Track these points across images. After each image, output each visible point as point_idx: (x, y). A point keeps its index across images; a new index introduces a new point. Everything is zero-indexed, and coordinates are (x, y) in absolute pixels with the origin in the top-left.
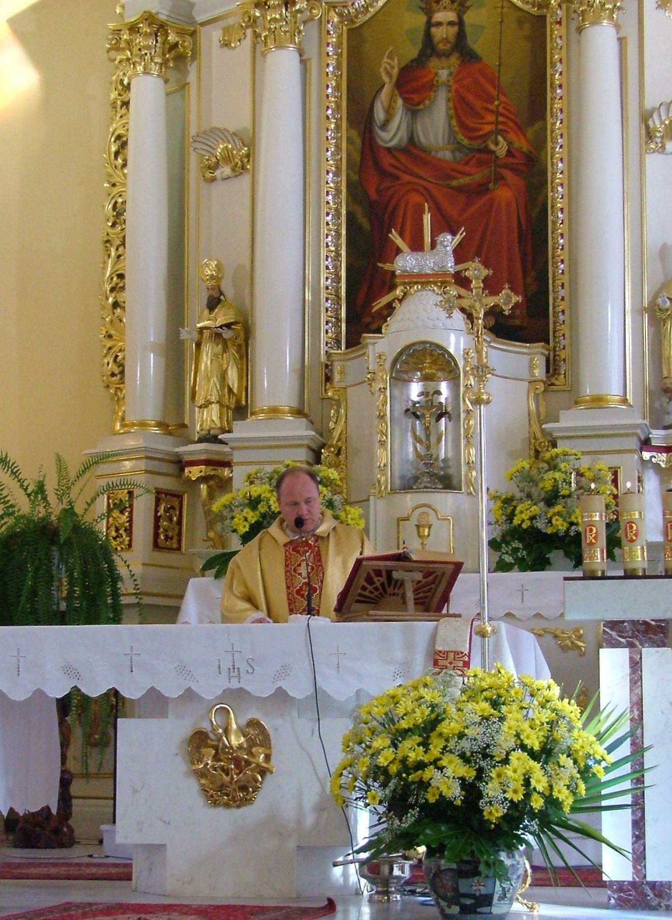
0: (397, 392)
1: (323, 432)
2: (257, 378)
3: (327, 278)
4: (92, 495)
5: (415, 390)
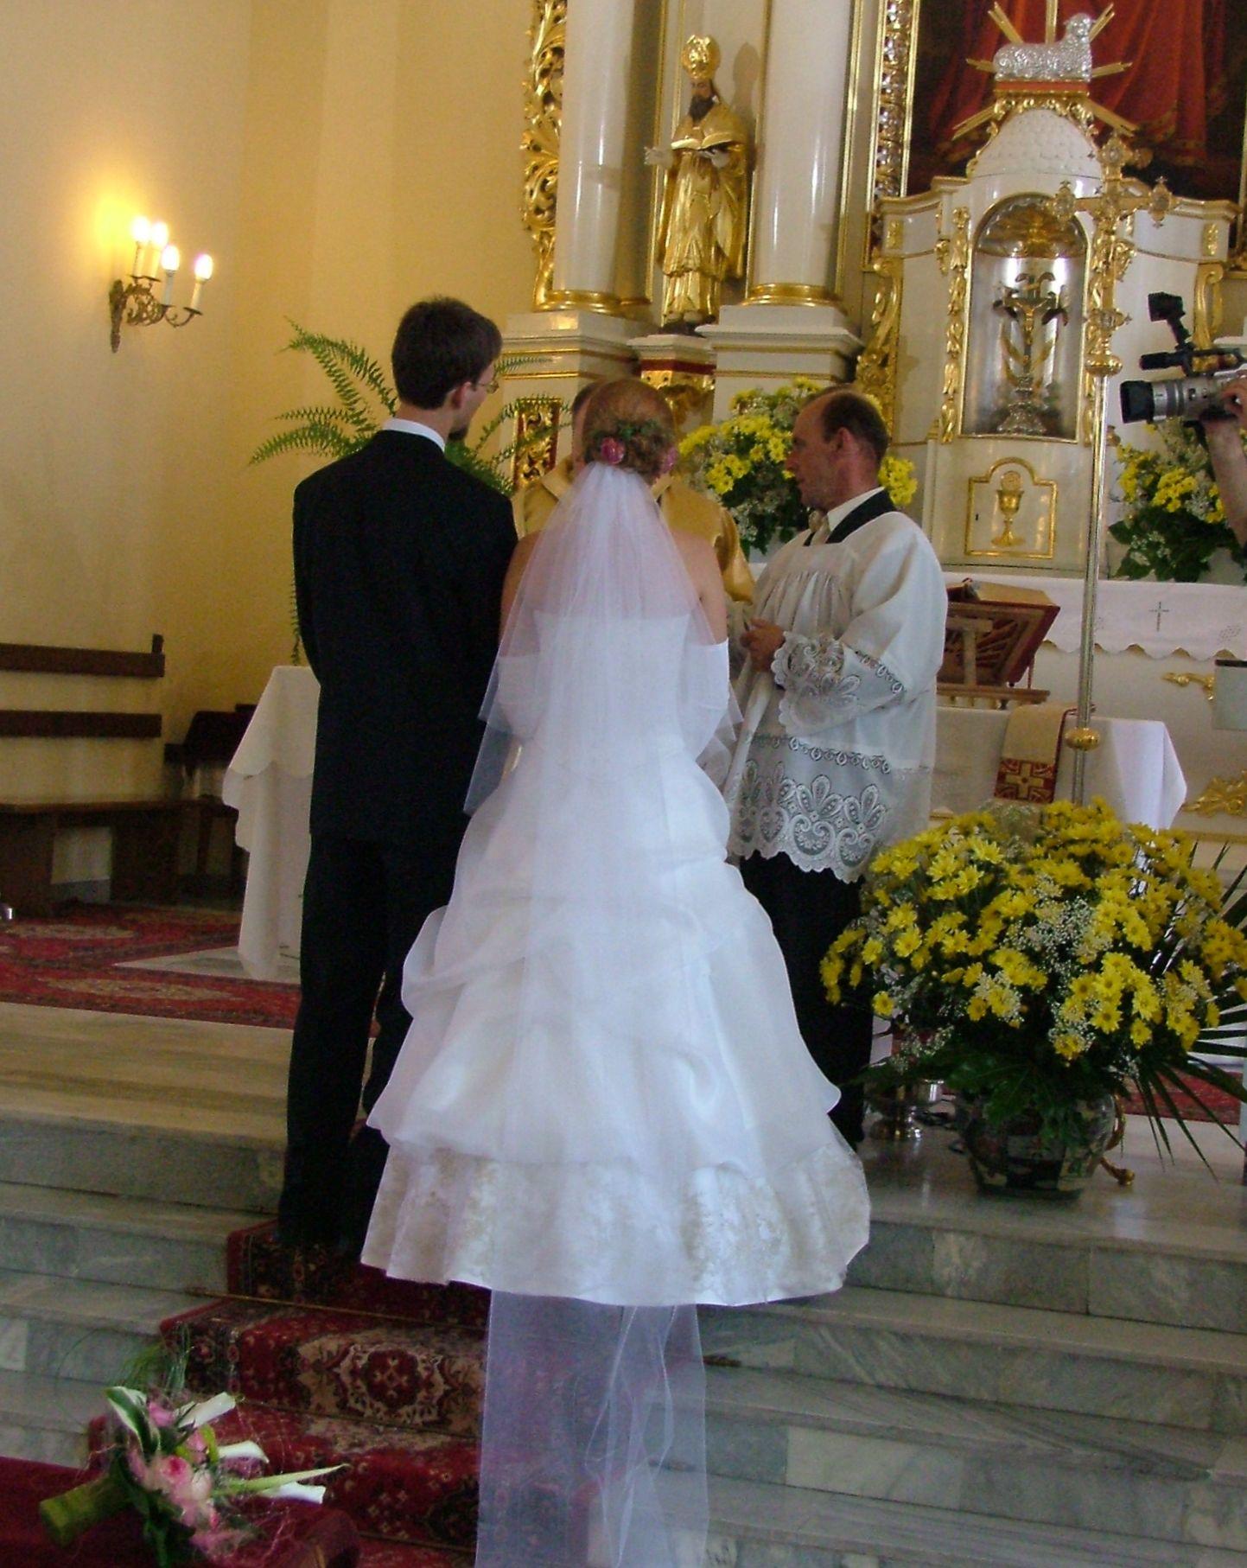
0: (981, 273)
1: (862, 328)
2: (764, 211)
3: (885, 76)
4: (494, 417)
5: (1012, 270)
